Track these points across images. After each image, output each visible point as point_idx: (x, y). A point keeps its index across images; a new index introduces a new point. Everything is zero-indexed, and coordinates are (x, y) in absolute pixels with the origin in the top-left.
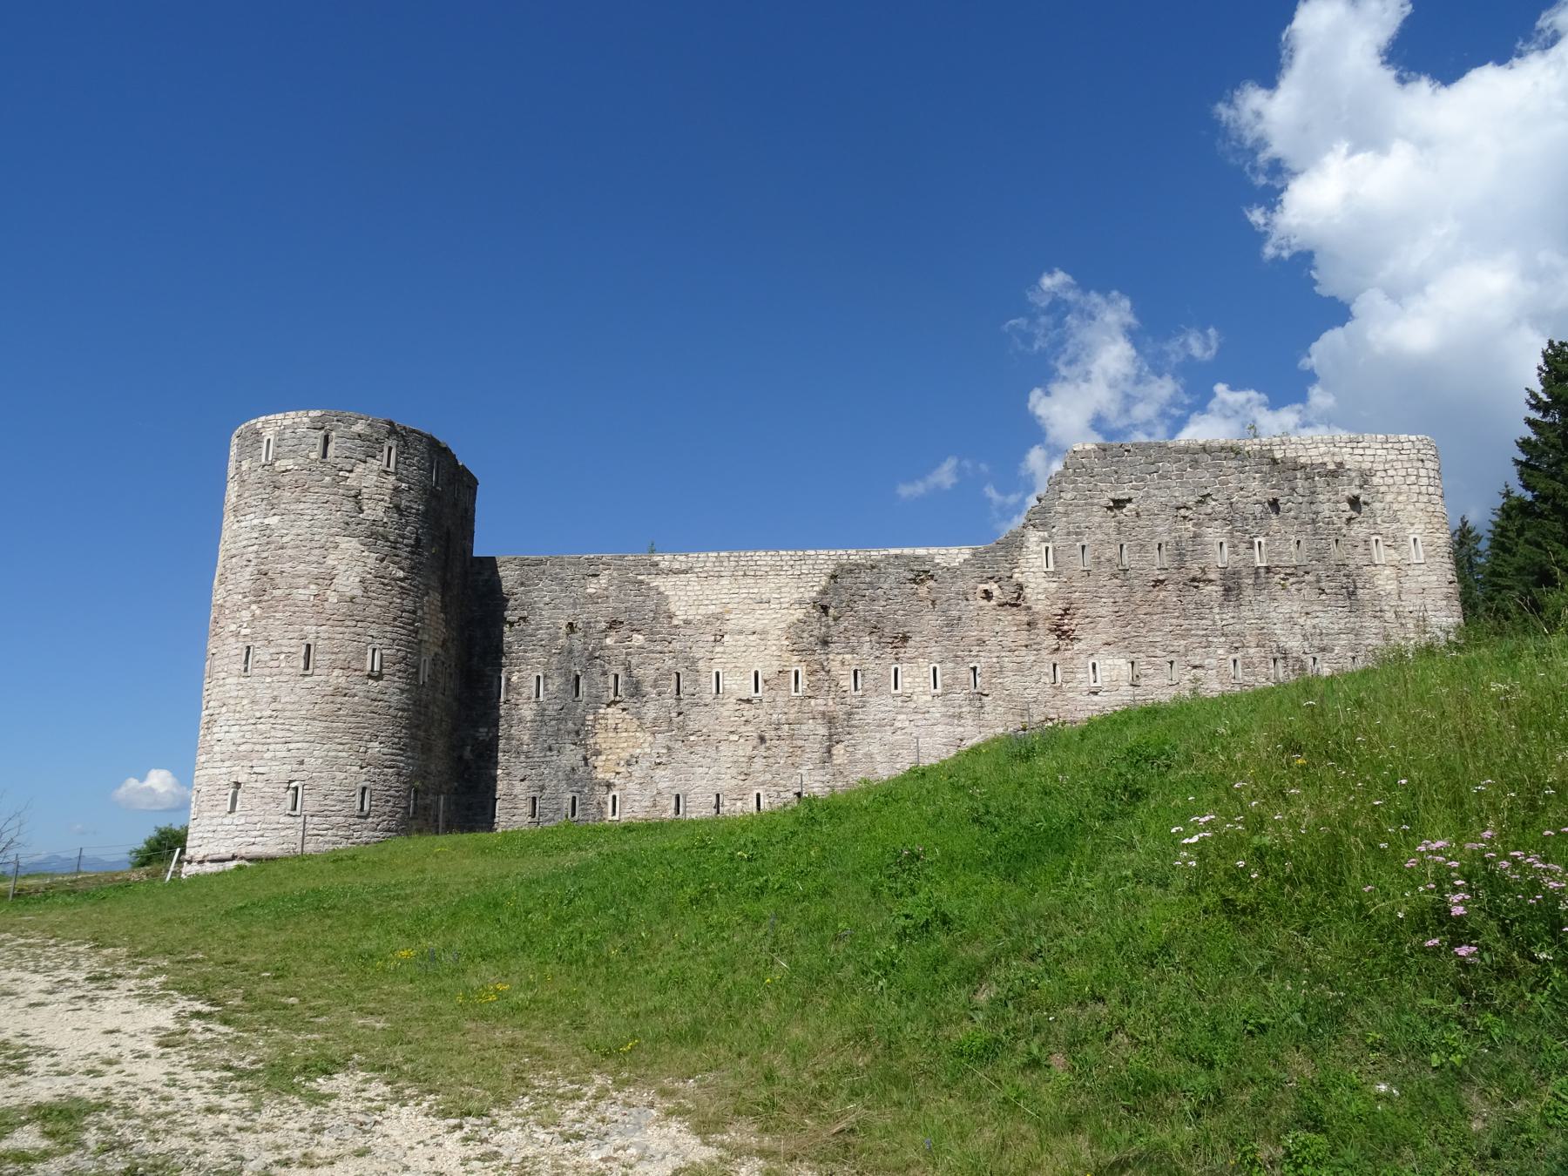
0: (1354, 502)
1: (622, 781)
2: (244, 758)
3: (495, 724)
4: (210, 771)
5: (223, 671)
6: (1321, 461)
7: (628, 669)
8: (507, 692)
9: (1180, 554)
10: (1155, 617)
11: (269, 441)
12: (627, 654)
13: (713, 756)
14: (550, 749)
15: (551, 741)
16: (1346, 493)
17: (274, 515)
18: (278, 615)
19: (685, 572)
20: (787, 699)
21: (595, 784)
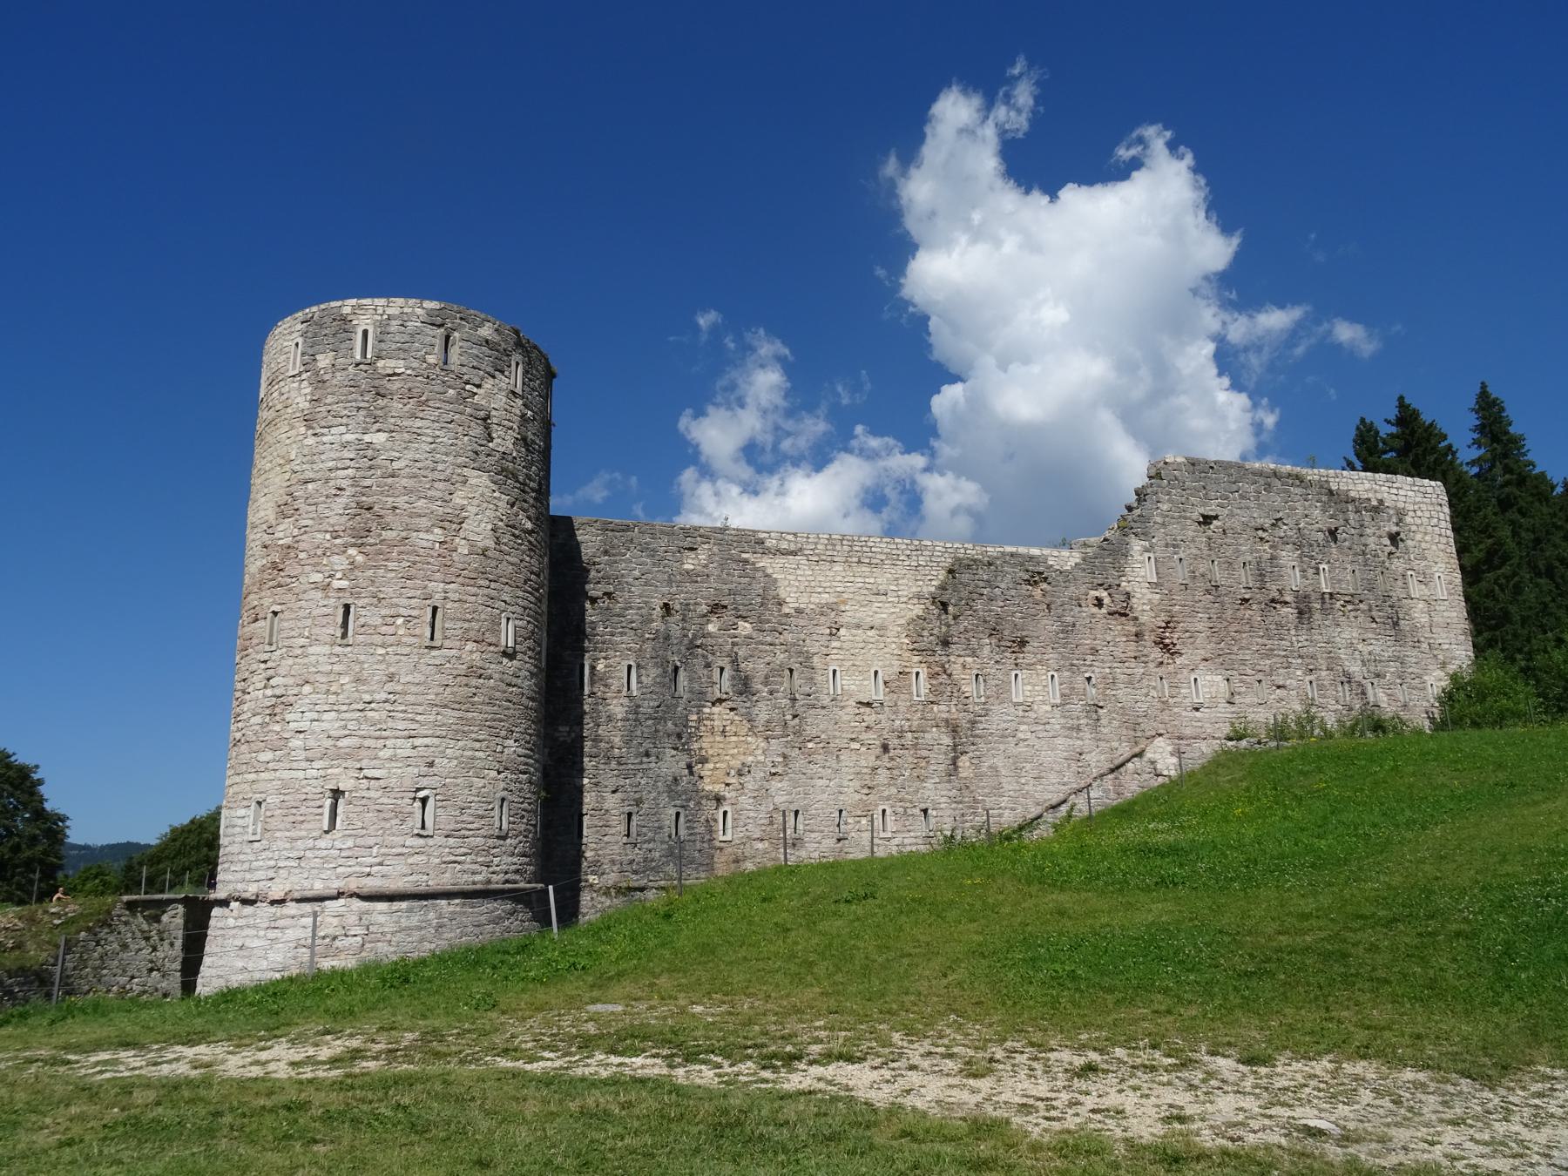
0: (1394, 538)
1: (734, 794)
2: (348, 756)
3: (579, 722)
4: (286, 775)
5: (301, 636)
6: (1366, 496)
7: (735, 662)
8: (592, 683)
9: (1261, 575)
10: (1244, 635)
11: (365, 333)
12: (734, 644)
13: (834, 766)
14: (647, 755)
15: (647, 745)
16: (1387, 529)
17: (379, 431)
18: (391, 565)
19: (794, 553)
20: (908, 704)
21: (702, 797)
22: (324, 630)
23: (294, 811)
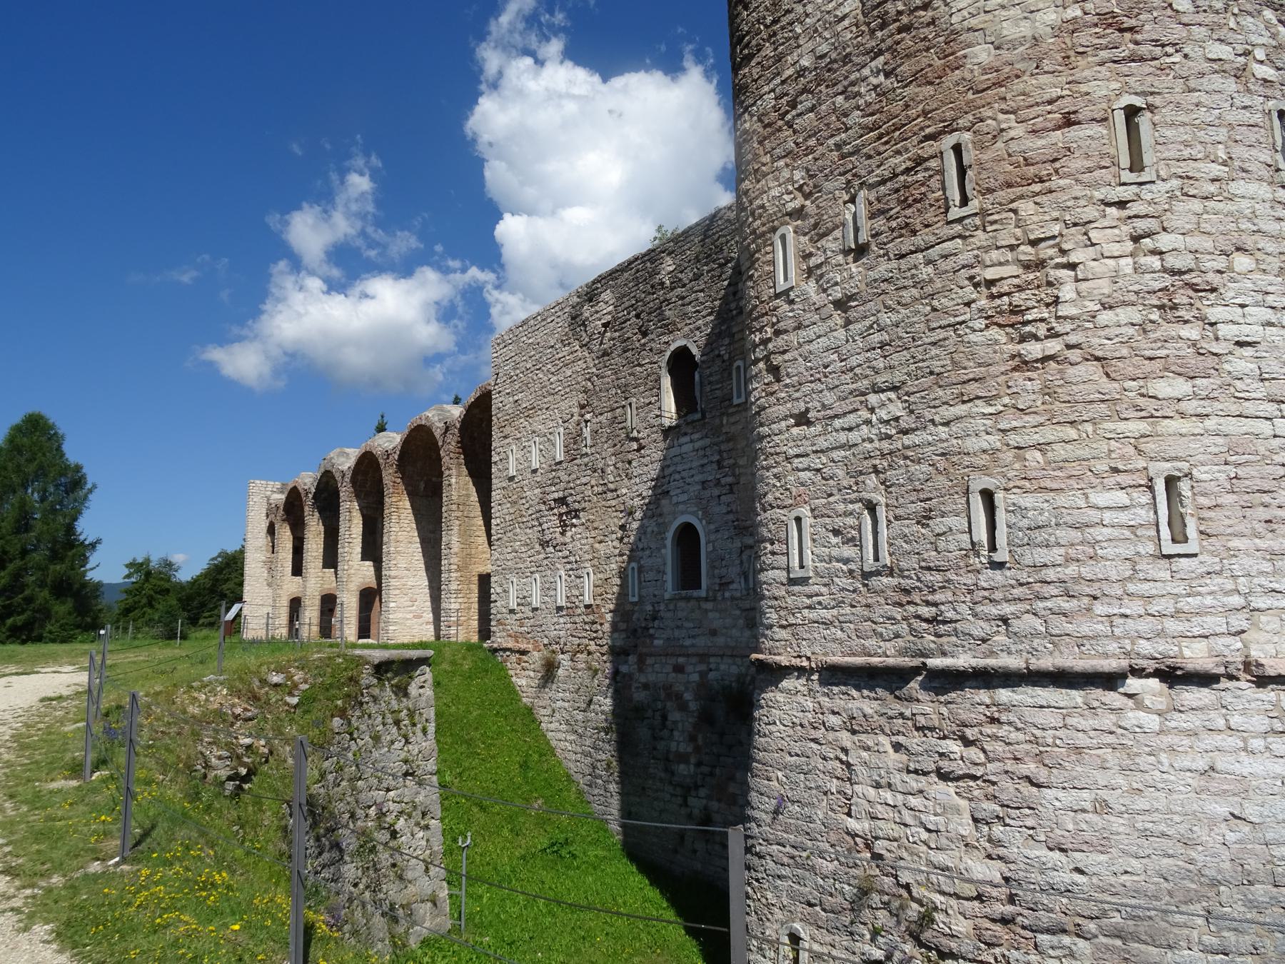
22: (1254, 152)
23: (1266, 498)
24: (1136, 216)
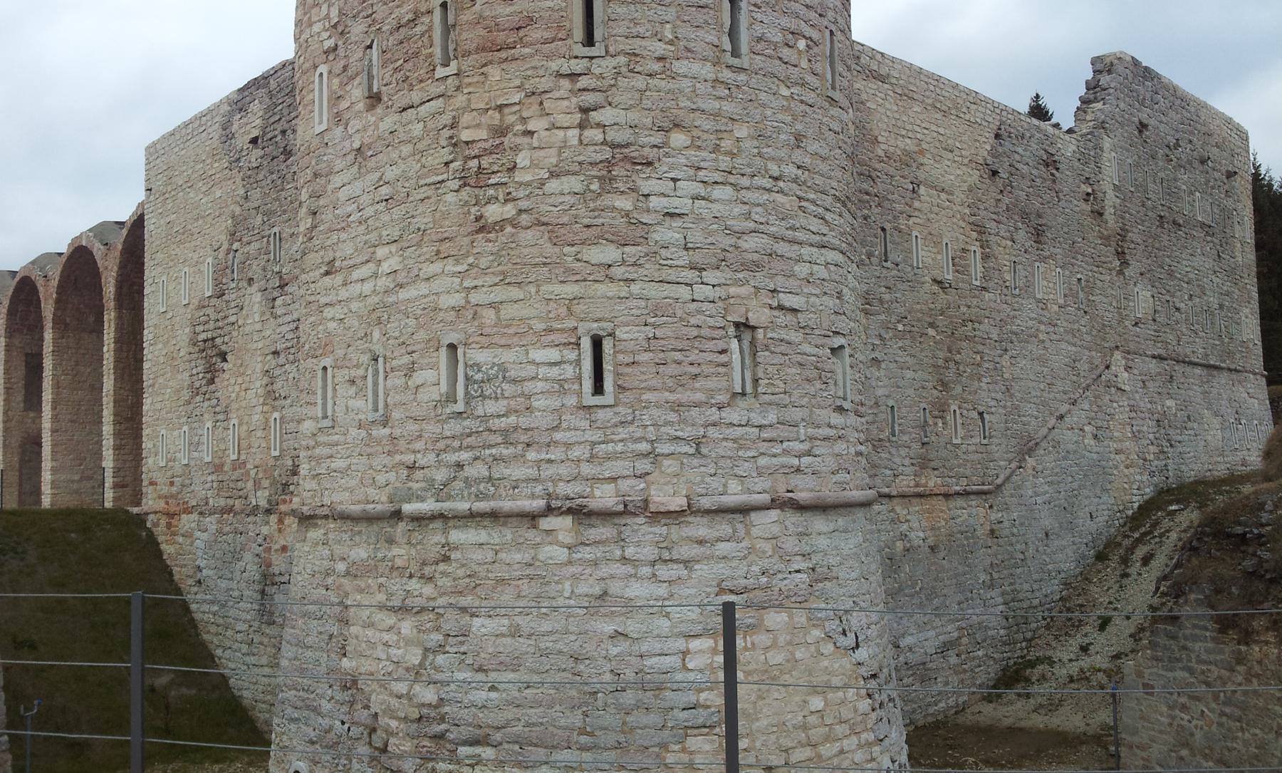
22: (701, 33)
24: (584, 90)
